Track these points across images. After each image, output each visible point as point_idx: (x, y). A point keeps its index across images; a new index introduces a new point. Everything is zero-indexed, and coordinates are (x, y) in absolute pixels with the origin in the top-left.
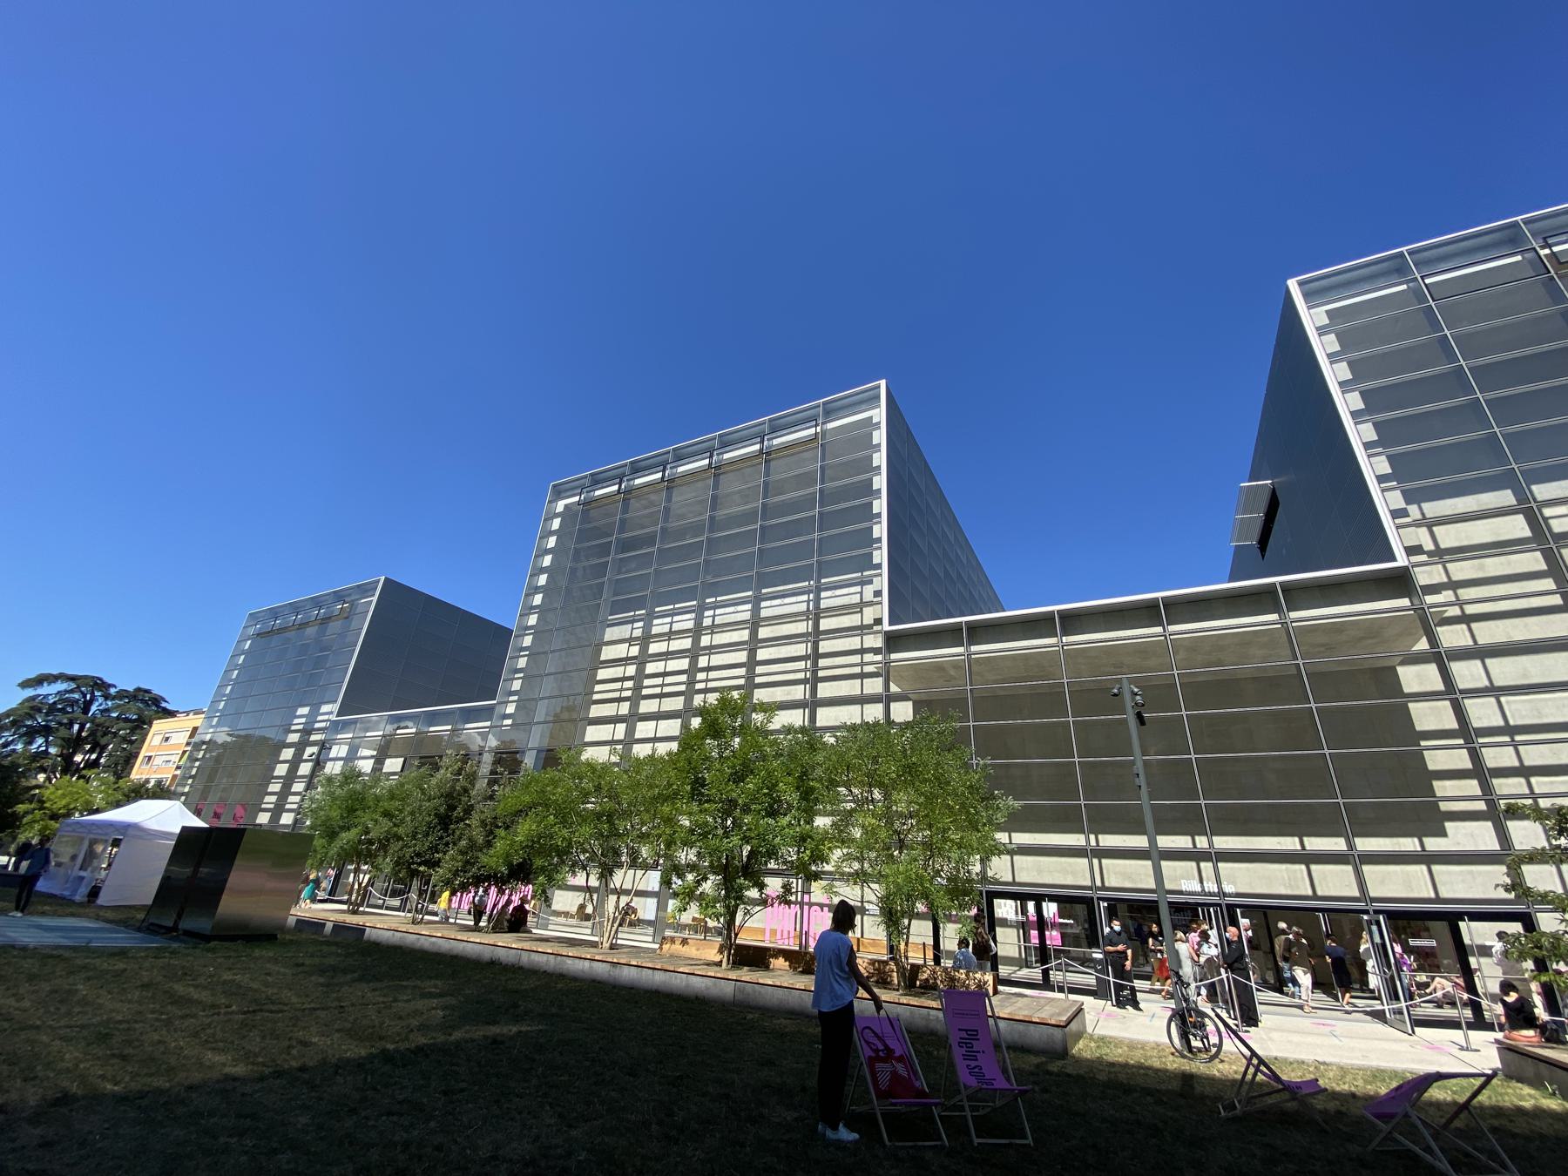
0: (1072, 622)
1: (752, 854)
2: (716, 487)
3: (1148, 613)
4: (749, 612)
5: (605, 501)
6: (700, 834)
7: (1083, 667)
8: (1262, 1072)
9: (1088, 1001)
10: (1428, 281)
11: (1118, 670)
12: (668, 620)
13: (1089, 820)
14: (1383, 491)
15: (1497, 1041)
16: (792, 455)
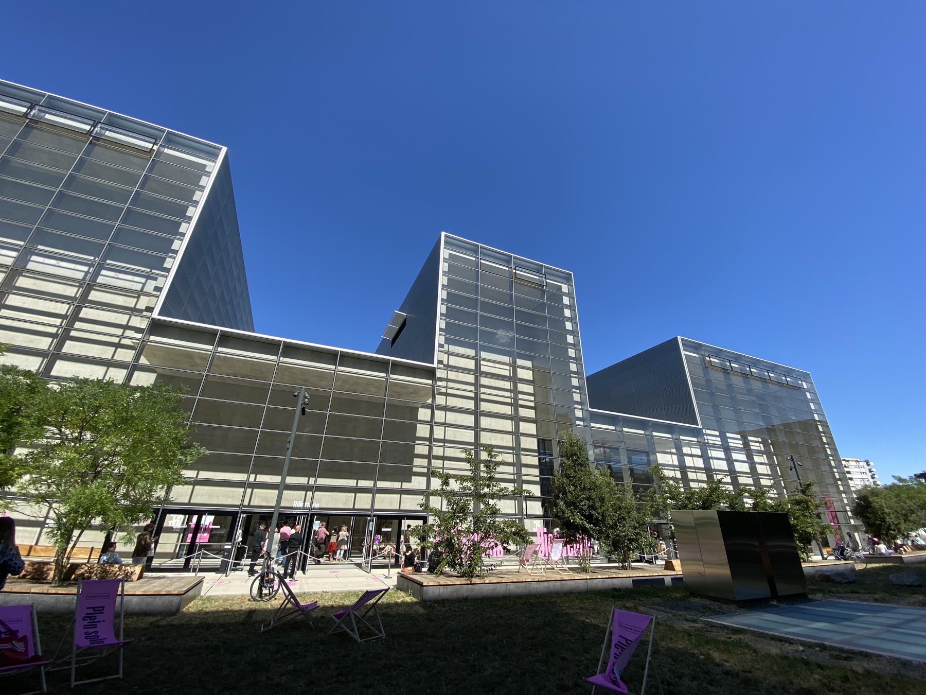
0: (291, 350)
4: (13, 259)
8: (291, 602)
10: (482, 261)
13: (254, 465)
14: (440, 335)
15: (398, 573)
16: (122, 152)
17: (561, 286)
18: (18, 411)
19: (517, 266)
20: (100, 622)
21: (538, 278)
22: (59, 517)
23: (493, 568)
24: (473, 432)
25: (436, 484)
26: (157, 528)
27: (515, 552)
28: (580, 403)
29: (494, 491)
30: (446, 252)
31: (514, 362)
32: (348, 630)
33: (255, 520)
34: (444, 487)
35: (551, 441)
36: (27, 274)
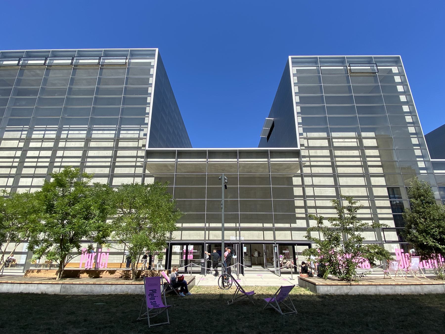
0: (212, 154)
1: (74, 235)
2: (74, 74)
3: (233, 154)
5: (9, 68)
6: (50, 226)
7: (213, 169)
9: (197, 275)
10: (322, 68)
11: (223, 171)
12: (43, 132)
13: (207, 218)
15: (298, 277)
17: (391, 69)
18: (104, 203)
19: (350, 64)
20: (156, 297)
21: (370, 68)
22: (131, 249)
23: (364, 275)
24: (334, 188)
25: (313, 223)
26: (169, 254)
27: (379, 265)
28: (422, 157)
29: (357, 226)
30: (294, 69)
31: (360, 135)
32: (275, 307)
33: (213, 247)
34: (320, 225)
35: (399, 188)
36: (93, 140)
